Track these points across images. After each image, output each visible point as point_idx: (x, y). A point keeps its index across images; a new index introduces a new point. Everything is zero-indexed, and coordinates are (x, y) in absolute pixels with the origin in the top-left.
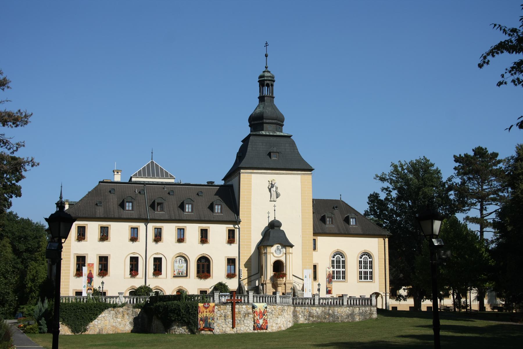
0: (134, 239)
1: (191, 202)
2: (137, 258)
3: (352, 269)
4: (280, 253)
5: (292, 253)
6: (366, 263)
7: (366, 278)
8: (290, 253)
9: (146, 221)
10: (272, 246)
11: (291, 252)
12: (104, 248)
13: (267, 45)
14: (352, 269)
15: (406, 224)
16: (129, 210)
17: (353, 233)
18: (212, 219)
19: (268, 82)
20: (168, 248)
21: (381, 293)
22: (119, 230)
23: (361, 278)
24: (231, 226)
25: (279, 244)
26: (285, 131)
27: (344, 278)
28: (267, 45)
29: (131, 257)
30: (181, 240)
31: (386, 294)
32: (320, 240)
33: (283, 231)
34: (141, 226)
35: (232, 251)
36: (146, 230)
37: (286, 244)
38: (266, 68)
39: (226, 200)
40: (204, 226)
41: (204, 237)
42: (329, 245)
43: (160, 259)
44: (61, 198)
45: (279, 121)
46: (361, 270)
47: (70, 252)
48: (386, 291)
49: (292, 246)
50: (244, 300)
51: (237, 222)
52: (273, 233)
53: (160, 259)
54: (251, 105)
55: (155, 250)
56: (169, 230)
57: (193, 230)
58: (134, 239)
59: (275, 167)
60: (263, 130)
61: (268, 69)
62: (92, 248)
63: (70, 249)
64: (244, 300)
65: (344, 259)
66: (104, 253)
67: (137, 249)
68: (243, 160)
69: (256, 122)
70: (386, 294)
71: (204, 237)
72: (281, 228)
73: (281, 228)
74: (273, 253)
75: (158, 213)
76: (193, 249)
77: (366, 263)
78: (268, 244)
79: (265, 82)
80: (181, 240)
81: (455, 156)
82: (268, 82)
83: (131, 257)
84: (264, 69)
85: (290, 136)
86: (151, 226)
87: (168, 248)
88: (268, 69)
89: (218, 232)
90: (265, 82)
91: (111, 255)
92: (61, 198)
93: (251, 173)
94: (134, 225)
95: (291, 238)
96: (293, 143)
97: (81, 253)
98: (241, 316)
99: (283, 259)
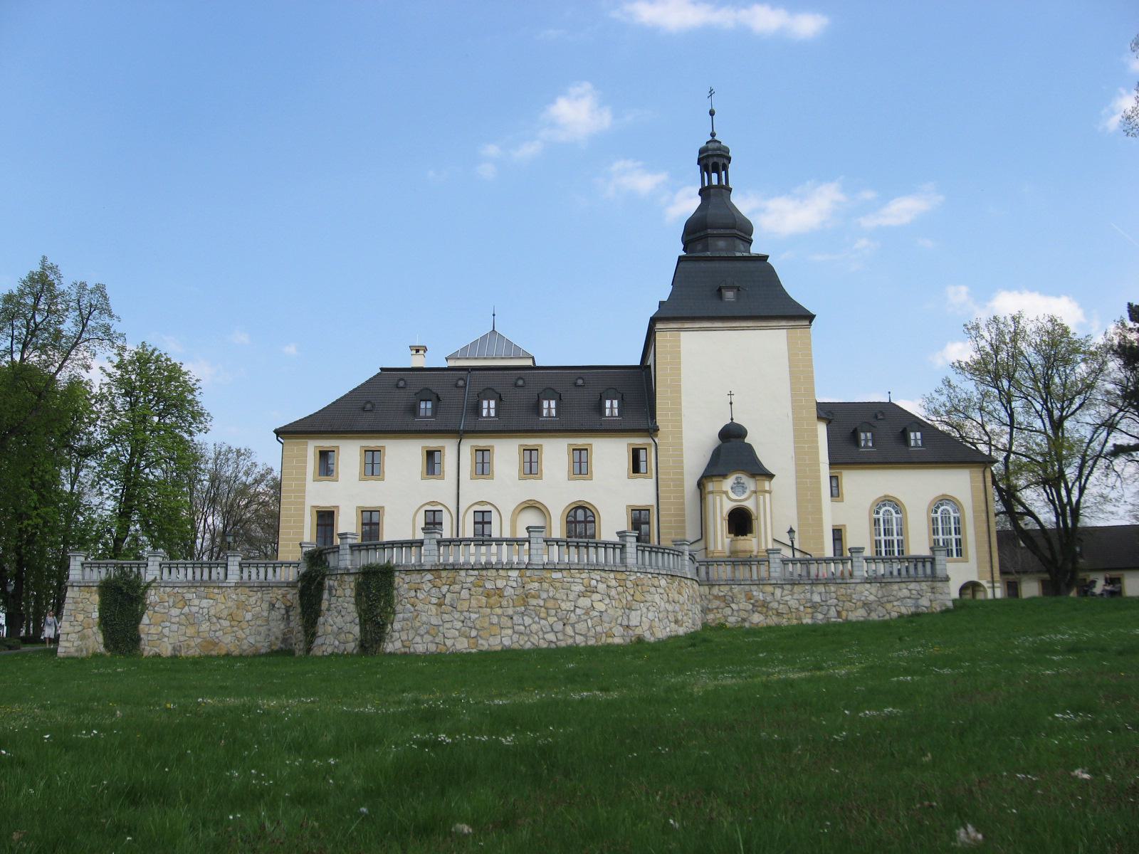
1: (869, 427)
4: (744, 492)
5: (770, 492)
6: (946, 519)
8: (766, 492)
9: (459, 434)
10: (724, 476)
11: (767, 488)
13: (711, 92)
16: (426, 417)
17: (916, 460)
18: (598, 427)
19: (715, 159)
21: (984, 582)
22: (403, 456)
24: (638, 441)
25: (736, 470)
26: (755, 249)
31: (993, 582)
32: (853, 480)
33: (750, 446)
34: (448, 447)
35: (642, 492)
37: (760, 473)
44: (713, 135)
45: (742, 231)
47: (303, 503)
48: (993, 578)
49: (770, 476)
51: (652, 431)
52: (733, 452)
54: (690, 203)
55: (475, 491)
56: (506, 452)
57: (555, 451)
59: (729, 314)
63: (304, 497)
68: (672, 314)
69: (695, 232)
70: (993, 582)
72: (747, 440)
73: (747, 440)
74: (726, 493)
77: (946, 519)
78: (715, 473)
79: (713, 160)
81: (1130, 305)
82: (715, 159)
84: (710, 138)
86: (468, 446)
89: (610, 454)
90: (713, 160)
91: (848, 529)
92: (713, 135)
93: (680, 330)
94: (433, 443)
95: (766, 458)
96: (771, 270)
97: (325, 503)
98: (504, 603)
99: (750, 504)
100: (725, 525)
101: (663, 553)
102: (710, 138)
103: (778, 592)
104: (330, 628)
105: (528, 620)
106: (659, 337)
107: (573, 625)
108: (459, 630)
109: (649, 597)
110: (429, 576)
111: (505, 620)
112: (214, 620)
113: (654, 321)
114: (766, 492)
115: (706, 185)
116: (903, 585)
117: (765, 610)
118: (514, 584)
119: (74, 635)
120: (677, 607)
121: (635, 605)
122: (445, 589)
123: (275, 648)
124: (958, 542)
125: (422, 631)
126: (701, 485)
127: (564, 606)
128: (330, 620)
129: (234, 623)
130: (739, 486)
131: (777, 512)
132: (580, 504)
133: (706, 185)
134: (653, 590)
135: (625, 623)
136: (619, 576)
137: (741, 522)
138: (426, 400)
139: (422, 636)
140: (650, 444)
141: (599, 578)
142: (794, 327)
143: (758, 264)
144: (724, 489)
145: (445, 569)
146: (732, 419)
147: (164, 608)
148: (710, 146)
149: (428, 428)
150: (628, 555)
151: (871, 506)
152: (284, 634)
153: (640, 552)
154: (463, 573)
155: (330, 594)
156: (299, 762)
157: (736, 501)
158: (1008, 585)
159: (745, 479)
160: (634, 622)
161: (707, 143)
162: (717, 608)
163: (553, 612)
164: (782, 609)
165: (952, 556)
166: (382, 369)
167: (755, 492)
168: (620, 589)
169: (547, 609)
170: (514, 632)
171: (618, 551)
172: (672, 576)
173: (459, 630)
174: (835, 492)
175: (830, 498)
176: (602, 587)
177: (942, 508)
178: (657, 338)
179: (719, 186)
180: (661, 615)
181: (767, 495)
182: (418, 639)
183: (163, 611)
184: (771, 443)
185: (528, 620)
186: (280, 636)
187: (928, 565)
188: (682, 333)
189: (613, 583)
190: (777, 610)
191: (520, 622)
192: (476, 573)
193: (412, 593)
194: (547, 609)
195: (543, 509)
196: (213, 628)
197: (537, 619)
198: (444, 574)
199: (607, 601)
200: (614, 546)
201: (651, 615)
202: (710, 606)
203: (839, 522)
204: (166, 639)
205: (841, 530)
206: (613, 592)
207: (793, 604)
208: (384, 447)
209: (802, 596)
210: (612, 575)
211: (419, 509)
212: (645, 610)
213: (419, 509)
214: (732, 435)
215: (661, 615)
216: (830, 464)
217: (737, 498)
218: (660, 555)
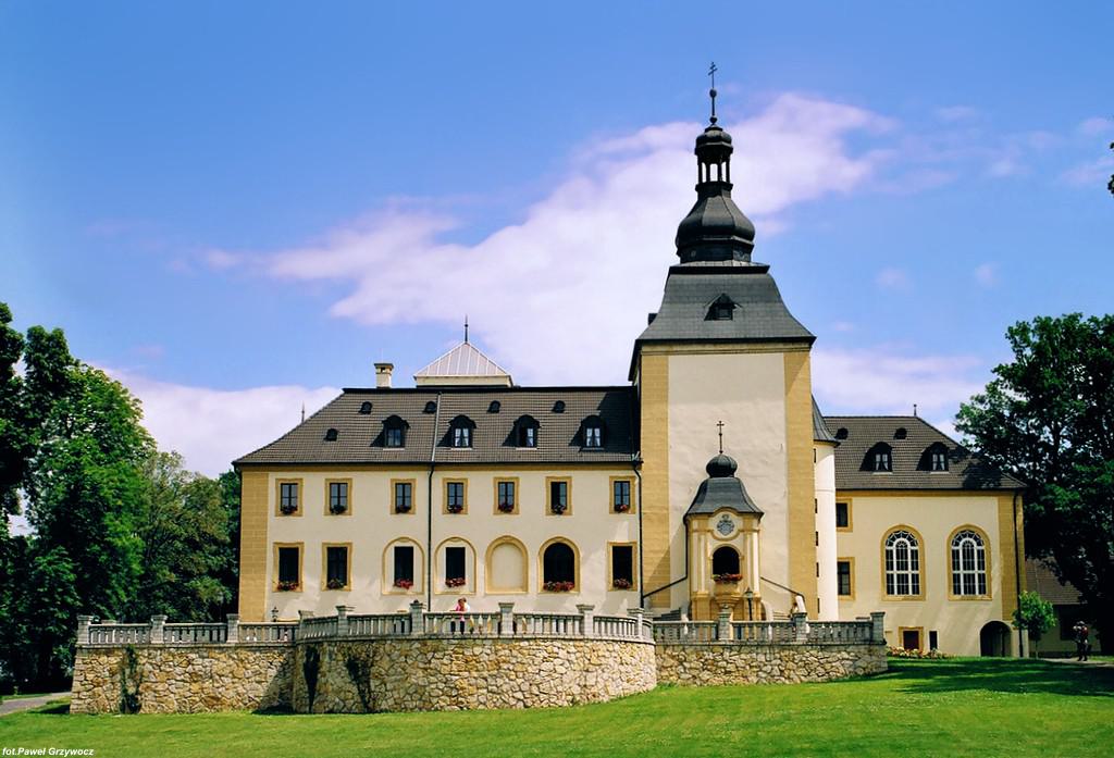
0: (403, 507)
2: (411, 549)
3: (936, 566)
5: (758, 531)
7: (903, 590)
8: (755, 531)
9: (432, 467)
10: (710, 514)
12: (338, 531)
13: (713, 69)
14: (936, 566)
15: (42, 449)
20: (478, 524)
21: (1009, 623)
22: (371, 491)
23: (890, 591)
26: (757, 258)
27: (916, 590)
28: (713, 69)
29: (397, 549)
30: (506, 507)
32: (859, 506)
34: (419, 479)
35: (623, 531)
36: (428, 490)
38: (713, 120)
39: (615, 422)
40: (559, 474)
41: (558, 500)
42: (877, 515)
43: (461, 551)
46: (915, 572)
50: (219, 634)
51: (636, 465)
53: (461, 551)
54: (716, 99)
55: (449, 529)
58: (403, 507)
60: (732, 259)
61: (718, 124)
62: (312, 531)
64: (219, 634)
65: (980, 548)
66: (337, 540)
67: (410, 528)
71: (558, 500)
74: (711, 531)
75: (457, 453)
76: (535, 525)
80: (506, 507)
83: (397, 549)
84: (709, 124)
85: (764, 269)
86: (440, 478)
87: (478, 524)
88: (718, 124)
89: (591, 488)
92: (713, 120)
93: (667, 353)
97: (288, 539)
99: (736, 544)
100: (710, 566)
101: (618, 622)
102: (709, 124)
103: (727, 654)
104: (331, 687)
105: (500, 682)
106: (645, 360)
107: (537, 685)
108: (442, 690)
109: (603, 661)
110: (417, 645)
111: (481, 682)
112: (217, 677)
113: (639, 343)
114: (755, 531)
115: (704, 180)
116: (843, 648)
117: (714, 668)
118: (489, 651)
119: (85, 693)
120: (629, 668)
121: (591, 668)
122: (430, 656)
123: (275, 704)
124: (982, 577)
125: (411, 691)
126: (686, 520)
127: (530, 669)
128: (331, 681)
129: (236, 680)
130: (725, 525)
131: (766, 558)
132: (559, 540)
133: (704, 180)
134: (607, 654)
135: (582, 683)
136: (577, 643)
137: (727, 563)
138: (395, 429)
139: (411, 695)
140: (634, 477)
141: (560, 645)
142: (791, 350)
143: (762, 276)
144: (711, 528)
145: (430, 639)
146: (721, 452)
147: (170, 666)
148: (710, 133)
149: (398, 460)
150: (586, 625)
151: (883, 538)
152: (282, 689)
153: (597, 624)
154: (445, 642)
155: (330, 657)
156: (1081, 553)
157: (723, 540)
158: (342, 548)
159: (732, 517)
160: (591, 681)
161: (707, 130)
162: (671, 667)
163: (521, 675)
164: (731, 667)
165: (908, 593)
166: (347, 391)
167: (743, 531)
168: (578, 655)
169: (516, 672)
170: (488, 692)
171: (577, 623)
172: (626, 642)
173: (442, 690)
174: (843, 521)
175: (835, 528)
176: (562, 653)
177: (964, 540)
178: (643, 363)
179: (720, 182)
180: (614, 676)
181: (755, 534)
182: (408, 697)
183: (168, 670)
184: (763, 485)
185: (500, 682)
186: (278, 691)
187: (867, 629)
188: (670, 357)
189: (573, 650)
190: (725, 668)
191: (493, 683)
192: (456, 642)
193: (403, 659)
194: (516, 672)
195: (520, 546)
196: (216, 685)
197: (507, 680)
198: (429, 643)
199: (567, 664)
200: (574, 618)
201: (605, 676)
202: (665, 664)
203: (845, 555)
204: (172, 695)
205: (848, 564)
206: (573, 657)
207: (740, 663)
208: (350, 479)
209: (748, 656)
210: (571, 643)
211: (390, 544)
212: (600, 671)
213: (390, 544)
214: (720, 469)
215: (614, 676)
216: (837, 490)
217: (724, 537)
218: (615, 624)
